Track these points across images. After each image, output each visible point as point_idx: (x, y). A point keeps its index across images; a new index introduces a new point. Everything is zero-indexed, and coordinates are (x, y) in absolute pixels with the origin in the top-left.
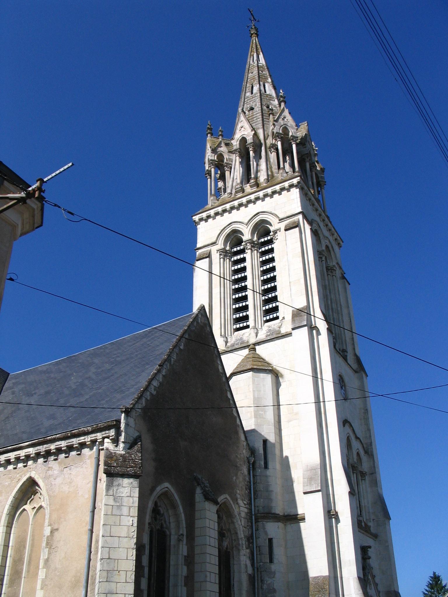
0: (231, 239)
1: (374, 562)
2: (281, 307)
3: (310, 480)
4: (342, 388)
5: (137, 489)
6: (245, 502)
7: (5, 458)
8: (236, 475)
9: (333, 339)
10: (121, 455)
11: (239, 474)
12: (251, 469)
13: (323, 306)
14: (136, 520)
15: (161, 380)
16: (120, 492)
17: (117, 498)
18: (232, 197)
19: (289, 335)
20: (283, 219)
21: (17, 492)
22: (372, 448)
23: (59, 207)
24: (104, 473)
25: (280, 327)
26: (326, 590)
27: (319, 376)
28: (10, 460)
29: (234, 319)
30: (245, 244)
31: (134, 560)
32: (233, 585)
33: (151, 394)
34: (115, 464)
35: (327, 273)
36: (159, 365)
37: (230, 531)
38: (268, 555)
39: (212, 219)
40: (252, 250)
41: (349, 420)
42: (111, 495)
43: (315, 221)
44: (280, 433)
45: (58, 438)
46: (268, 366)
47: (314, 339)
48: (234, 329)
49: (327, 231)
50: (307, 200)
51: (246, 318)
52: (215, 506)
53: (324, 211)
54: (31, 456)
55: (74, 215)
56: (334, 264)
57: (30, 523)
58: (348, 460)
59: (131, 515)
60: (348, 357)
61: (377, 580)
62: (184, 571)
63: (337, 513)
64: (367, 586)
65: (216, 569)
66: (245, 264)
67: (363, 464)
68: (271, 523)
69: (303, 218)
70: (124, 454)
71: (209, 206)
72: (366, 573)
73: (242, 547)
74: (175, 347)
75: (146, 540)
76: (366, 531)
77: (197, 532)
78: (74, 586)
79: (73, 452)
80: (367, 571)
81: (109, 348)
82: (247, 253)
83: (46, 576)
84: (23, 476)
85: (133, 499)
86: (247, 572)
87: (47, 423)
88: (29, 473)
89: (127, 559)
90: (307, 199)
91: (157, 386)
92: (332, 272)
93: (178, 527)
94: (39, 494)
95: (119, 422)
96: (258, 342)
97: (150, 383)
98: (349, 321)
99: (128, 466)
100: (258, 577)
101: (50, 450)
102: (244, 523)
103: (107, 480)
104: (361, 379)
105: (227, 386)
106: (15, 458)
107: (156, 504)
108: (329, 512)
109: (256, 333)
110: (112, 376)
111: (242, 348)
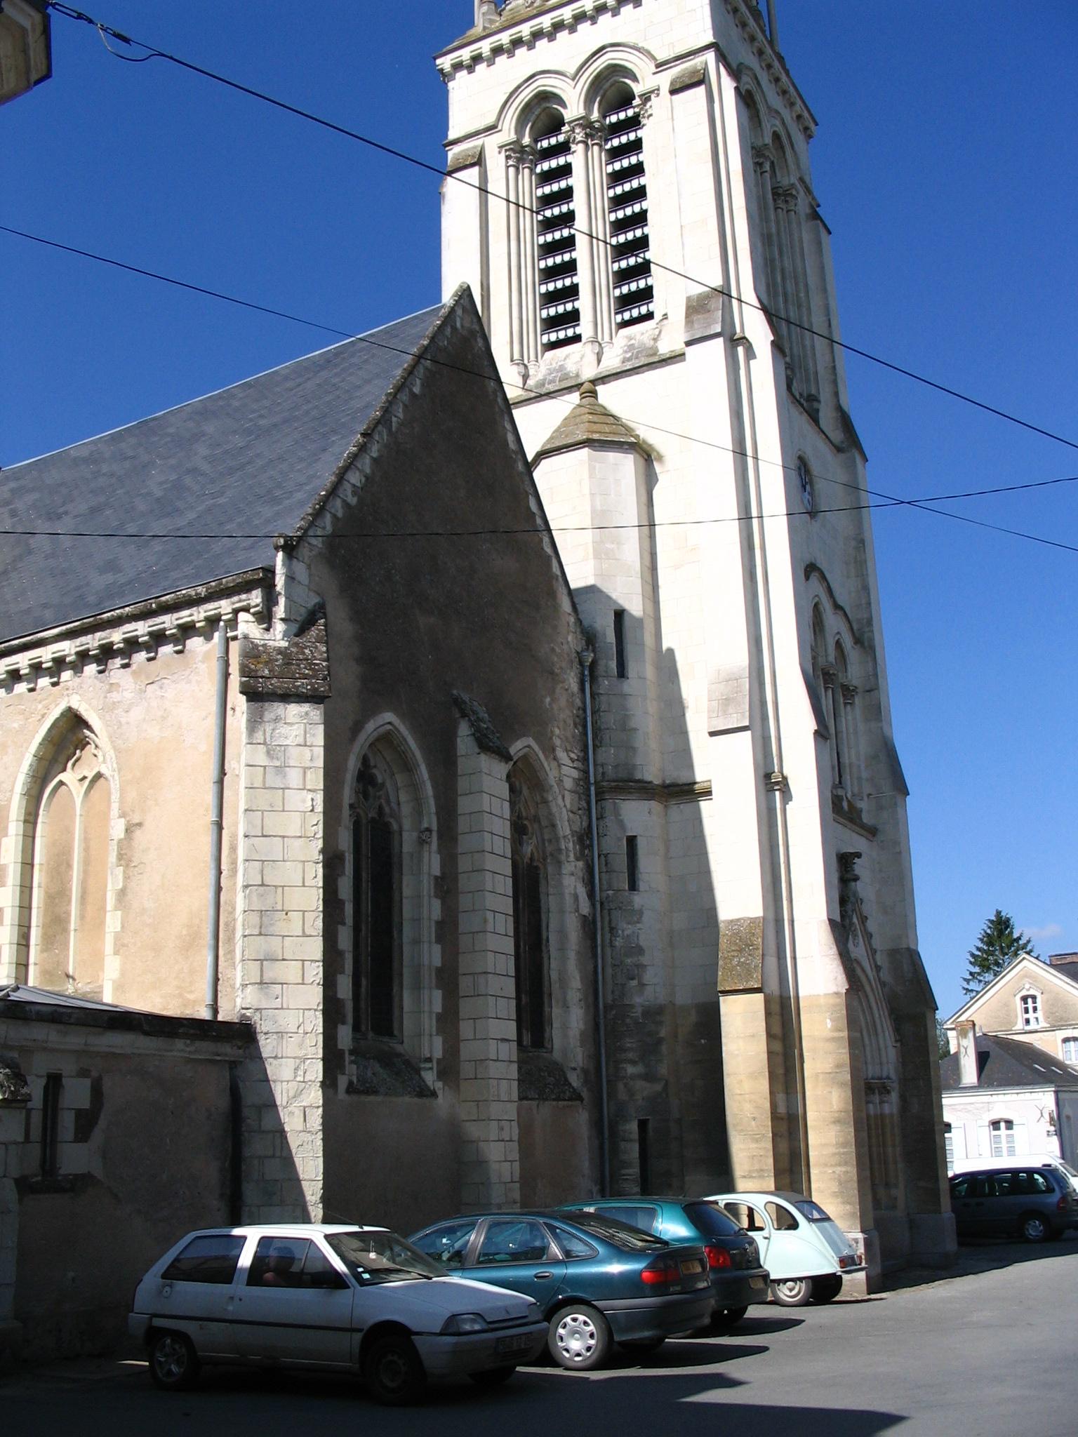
0: (533, 118)
1: (865, 888)
2: (657, 279)
3: (726, 703)
4: (804, 487)
5: (321, 727)
6: (573, 755)
7: (7, 666)
8: (552, 692)
9: (786, 368)
10: (280, 651)
11: (558, 691)
12: (587, 679)
13: (763, 288)
14: (320, 798)
15: (368, 471)
16: (280, 737)
17: (274, 751)
18: (535, 5)
19: (678, 358)
20: (665, 65)
21: (40, 744)
22: (873, 631)
23: (91, 21)
24: (241, 692)
25: (655, 340)
26: (755, 947)
27: (749, 452)
28: (17, 671)
29: (543, 320)
30: (569, 129)
31: (320, 887)
32: (548, 940)
33: (346, 504)
34: (267, 672)
35: (775, 205)
36: (362, 434)
37: (539, 822)
38: (626, 874)
39: (485, 64)
40: (587, 145)
41: (818, 565)
42: (260, 744)
43: (751, 69)
44: (654, 592)
45: (127, 615)
46: (626, 435)
47: (739, 369)
48: (543, 345)
49: (778, 94)
50: (729, 13)
51: (574, 317)
52: (503, 764)
53: (771, 43)
54: (68, 659)
55: (131, 42)
56: (792, 182)
57: (78, 812)
58: (814, 658)
59: (308, 787)
60: (821, 414)
61: (871, 926)
62: (435, 909)
63: (785, 778)
64: (847, 939)
65: (507, 905)
66: (571, 181)
67: (849, 667)
68: (633, 802)
69: (717, 62)
70: (285, 648)
71: (478, 30)
72: (846, 912)
73: (568, 856)
74: (399, 389)
75: (345, 842)
76: (851, 820)
77: (463, 824)
78: (188, 946)
79: (165, 647)
80: (849, 907)
81: (241, 395)
82: (574, 152)
83: (123, 927)
84: (52, 706)
85: (311, 750)
86: (577, 910)
87: (100, 581)
88: (66, 699)
89: (304, 886)
90: (729, 8)
91: (359, 485)
92: (787, 202)
93: (418, 813)
94: (93, 746)
95: (270, 571)
96: (603, 375)
97: (342, 478)
98: (827, 325)
99: (297, 675)
100: (602, 922)
101: (112, 644)
102: (571, 803)
103: (248, 708)
104: (851, 468)
105: (527, 482)
106: (30, 666)
107: (365, 760)
108: (768, 776)
109: (598, 353)
110: (249, 463)
111: (564, 391)
